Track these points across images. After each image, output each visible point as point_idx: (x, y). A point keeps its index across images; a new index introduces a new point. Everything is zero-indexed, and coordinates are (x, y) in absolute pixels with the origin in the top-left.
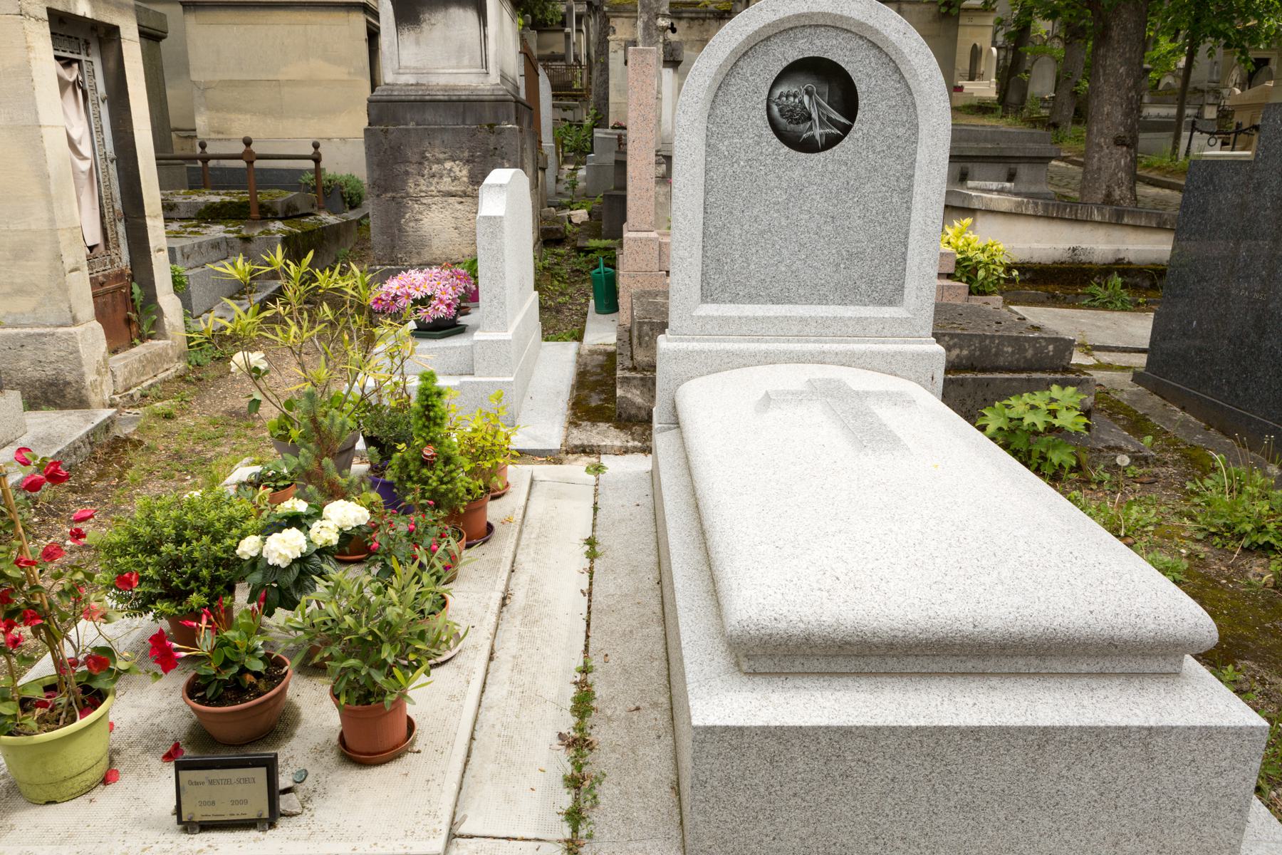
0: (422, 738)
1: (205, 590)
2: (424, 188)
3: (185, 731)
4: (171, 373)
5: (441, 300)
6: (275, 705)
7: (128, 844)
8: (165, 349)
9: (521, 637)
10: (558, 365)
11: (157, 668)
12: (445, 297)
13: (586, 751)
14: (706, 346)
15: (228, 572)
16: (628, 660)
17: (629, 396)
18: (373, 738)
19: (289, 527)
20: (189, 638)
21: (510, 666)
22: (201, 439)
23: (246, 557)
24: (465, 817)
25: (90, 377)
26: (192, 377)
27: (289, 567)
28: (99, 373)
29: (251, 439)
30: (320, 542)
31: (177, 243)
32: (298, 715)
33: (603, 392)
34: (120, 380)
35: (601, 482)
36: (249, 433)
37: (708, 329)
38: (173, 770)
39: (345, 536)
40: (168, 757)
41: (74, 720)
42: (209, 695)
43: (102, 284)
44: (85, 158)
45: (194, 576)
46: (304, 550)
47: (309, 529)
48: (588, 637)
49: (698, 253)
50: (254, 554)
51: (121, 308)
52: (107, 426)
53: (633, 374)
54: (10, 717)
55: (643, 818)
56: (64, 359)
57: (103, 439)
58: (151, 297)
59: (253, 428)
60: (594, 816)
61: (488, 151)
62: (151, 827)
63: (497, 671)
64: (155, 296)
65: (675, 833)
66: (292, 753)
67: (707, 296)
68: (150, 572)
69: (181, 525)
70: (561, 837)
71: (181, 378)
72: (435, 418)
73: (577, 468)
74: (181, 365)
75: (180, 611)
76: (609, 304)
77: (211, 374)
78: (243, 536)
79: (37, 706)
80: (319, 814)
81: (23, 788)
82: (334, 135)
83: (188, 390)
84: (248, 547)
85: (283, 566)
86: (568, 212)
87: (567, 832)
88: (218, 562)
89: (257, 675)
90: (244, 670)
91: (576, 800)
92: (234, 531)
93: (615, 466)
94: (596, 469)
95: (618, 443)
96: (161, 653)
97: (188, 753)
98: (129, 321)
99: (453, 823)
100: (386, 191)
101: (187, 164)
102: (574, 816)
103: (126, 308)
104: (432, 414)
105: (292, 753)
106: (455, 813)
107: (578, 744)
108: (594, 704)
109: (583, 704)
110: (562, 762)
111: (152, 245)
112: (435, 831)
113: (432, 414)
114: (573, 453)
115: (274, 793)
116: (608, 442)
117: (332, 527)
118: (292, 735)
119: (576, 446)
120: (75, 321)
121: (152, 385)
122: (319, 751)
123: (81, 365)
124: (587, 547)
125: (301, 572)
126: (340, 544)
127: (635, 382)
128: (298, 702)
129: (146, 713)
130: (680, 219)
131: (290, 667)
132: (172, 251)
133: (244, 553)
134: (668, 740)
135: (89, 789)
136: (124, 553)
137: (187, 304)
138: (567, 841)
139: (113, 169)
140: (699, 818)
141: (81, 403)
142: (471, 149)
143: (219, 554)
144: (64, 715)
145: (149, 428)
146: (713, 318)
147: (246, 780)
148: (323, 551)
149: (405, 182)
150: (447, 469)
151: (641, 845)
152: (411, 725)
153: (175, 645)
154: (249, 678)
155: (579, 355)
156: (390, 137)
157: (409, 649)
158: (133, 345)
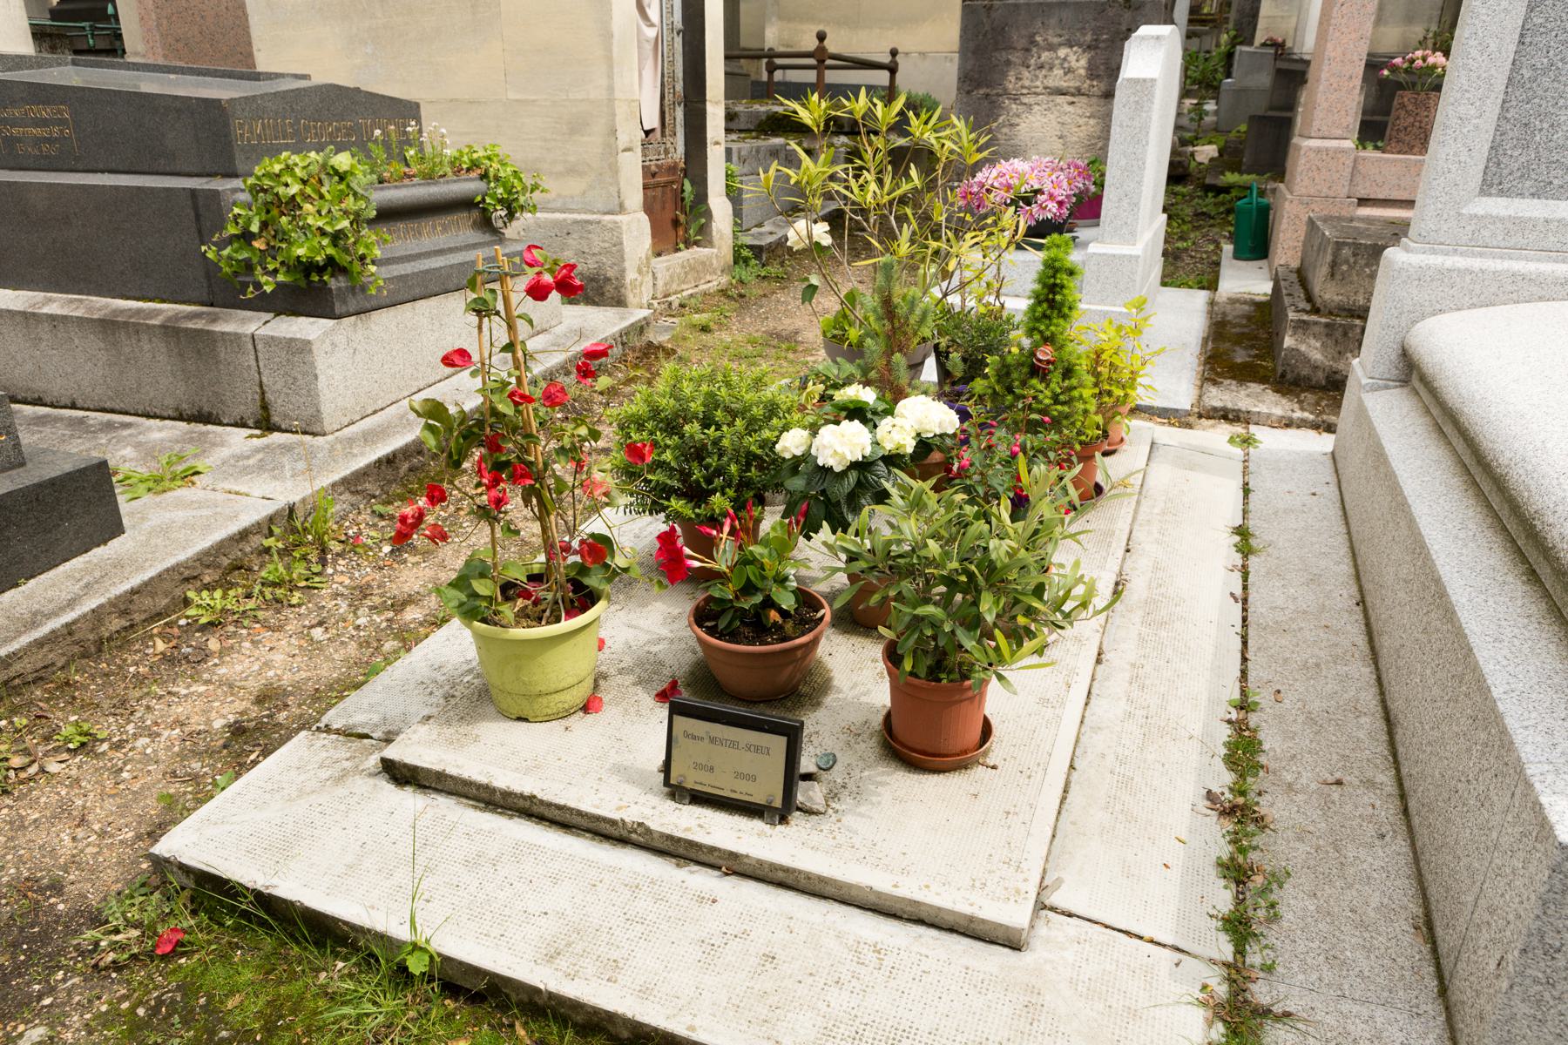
0: (997, 749)
1: (731, 492)
2: (1027, 83)
3: (686, 668)
4: (713, 286)
5: (1051, 196)
6: (804, 657)
7: (600, 795)
8: (709, 258)
9: (1142, 639)
10: (1183, 317)
11: (665, 581)
12: (1056, 192)
13: (1251, 828)
14: (1476, 263)
15: (761, 476)
16: (1316, 706)
17: (1303, 348)
18: (930, 733)
19: (851, 419)
20: (706, 547)
21: (1127, 675)
22: (738, 357)
23: (788, 456)
24: (1059, 881)
25: (631, 275)
26: (734, 292)
27: (844, 473)
28: (640, 271)
29: (791, 362)
30: (889, 446)
31: (735, 146)
32: (829, 680)
33: (1253, 347)
34: (660, 283)
35: (1252, 457)
36: (791, 356)
37: (1478, 238)
38: (666, 713)
39: (924, 446)
40: (662, 696)
41: (558, 620)
42: (721, 627)
43: (654, 175)
44: (652, 25)
45: (719, 472)
46: (868, 452)
47: (875, 426)
48: (1245, 660)
49: (1492, 110)
50: (799, 453)
51: (669, 205)
52: (641, 328)
53: (1314, 318)
54: (484, 598)
55: (1364, 964)
56: (607, 252)
57: (638, 343)
58: (702, 196)
59: (795, 351)
60: (1272, 935)
61: (1118, 33)
62: (631, 781)
63: (1107, 679)
64: (706, 195)
65: (1431, 1007)
66: (818, 728)
67: (1492, 184)
68: (668, 456)
69: (712, 402)
70: (1217, 956)
71: (723, 292)
72: (1062, 304)
73: (1218, 436)
74: (724, 279)
75: (698, 515)
76: (1257, 246)
77: (755, 292)
78: (786, 428)
79: (519, 596)
80: (848, 820)
81: (494, 692)
82: (913, 49)
83: (727, 306)
84: (792, 443)
85: (838, 469)
86: (1191, 149)
87: (1227, 951)
88: (750, 459)
89: (784, 614)
90: (769, 603)
91: (1240, 901)
92: (775, 421)
93: (1270, 440)
94: (1244, 441)
95: (1278, 411)
96: (669, 564)
97: (685, 695)
98: (676, 223)
99: (1042, 888)
100: (979, 86)
101: (756, 72)
102: (1238, 927)
103: (676, 210)
104: (1058, 297)
105: (818, 728)
106: (1045, 871)
107: (1239, 813)
108: (1263, 759)
109: (1243, 752)
110: (1214, 838)
111: (709, 135)
112: (1018, 892)
113: (1058, 297)
114: (1209, 418)
115: (792, 776)
116: (1263, 408)
117: (908, 428)
118: (819, 704)
119: (1215, 409)
120: (621, 209)
121: (691, 295)
122: (853, 734)
123: (623, 260)
124: (1237, 538)
125: (859, 483)
126: (914, 456)
127: (1316, 329)
128: (830, 662)
129: (644, 638)
130: (1474, 53)
131: (826, 612)
132: (728, 152)
133: (785, 449)
134: (1401, 845)
135: (566, 714)
136: (640, 427)
137: (737, 213)
138: (1227, 965)
139: (679, 41)
140: (1523, 1009)
141: (619, 302)
142: (1097, 31)
143: (753, 448)
144: (548, 613)
145: (684, 339)
146: (1496, 219)
147: (758, 749)
148: (892, 460)
149: (1004, 75)
150: (1067, 383)
151: (1365, 1012)
152: (987, 730)
153: (687, 551)
154: (774, 615)
155: (1212, 303)
156: (994, 15)
157: (1017, 610)
158: (678, 250)
